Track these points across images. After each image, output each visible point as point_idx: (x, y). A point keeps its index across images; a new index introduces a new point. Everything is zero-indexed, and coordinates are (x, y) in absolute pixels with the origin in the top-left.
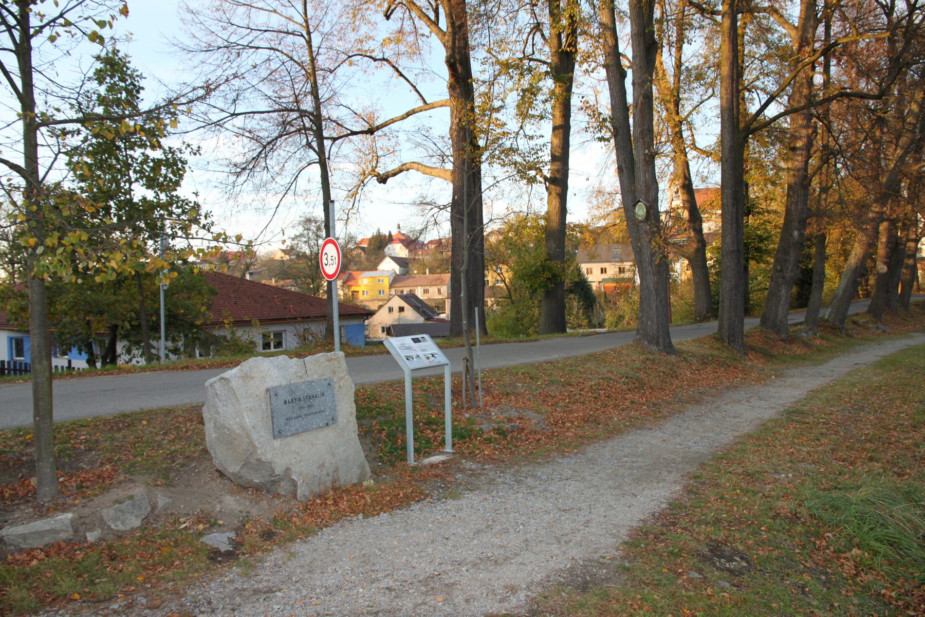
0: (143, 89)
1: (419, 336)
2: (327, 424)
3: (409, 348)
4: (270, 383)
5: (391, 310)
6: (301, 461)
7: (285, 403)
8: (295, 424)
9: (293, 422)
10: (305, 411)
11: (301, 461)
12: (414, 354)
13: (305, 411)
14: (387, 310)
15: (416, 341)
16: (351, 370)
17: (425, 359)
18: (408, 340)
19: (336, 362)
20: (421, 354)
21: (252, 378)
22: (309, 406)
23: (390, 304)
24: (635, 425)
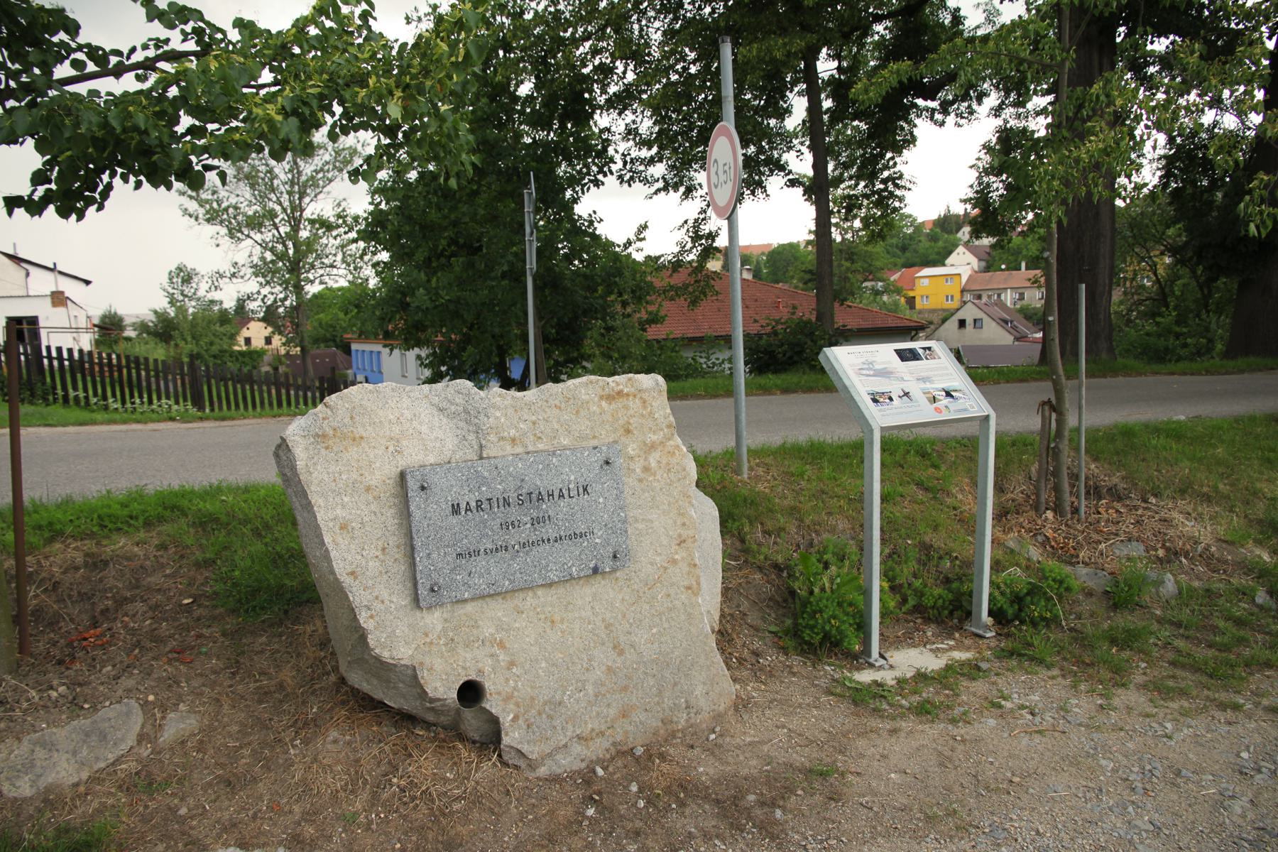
0: (961, 201)
1: (916, 345)
2: (596, 570)
3: (885, 373)
4: (413, 456)
5: (962, 323)
6: (512, 664)
7: (455, 510)
8: (489, 570)
9: (481, 562)
10: (525, 533)
11: (512, 664)
12: (895, 389)
13: (515, 537)
14: (957, 324)
15: (905, 356)
16: (682, 428)
17: (923, 401)
18: (885, 353)
19: (634, 404)
20: (915, 389)
21: (357, 440)
22: (536, 521)
23: (960, 315)
24: (571, 377)
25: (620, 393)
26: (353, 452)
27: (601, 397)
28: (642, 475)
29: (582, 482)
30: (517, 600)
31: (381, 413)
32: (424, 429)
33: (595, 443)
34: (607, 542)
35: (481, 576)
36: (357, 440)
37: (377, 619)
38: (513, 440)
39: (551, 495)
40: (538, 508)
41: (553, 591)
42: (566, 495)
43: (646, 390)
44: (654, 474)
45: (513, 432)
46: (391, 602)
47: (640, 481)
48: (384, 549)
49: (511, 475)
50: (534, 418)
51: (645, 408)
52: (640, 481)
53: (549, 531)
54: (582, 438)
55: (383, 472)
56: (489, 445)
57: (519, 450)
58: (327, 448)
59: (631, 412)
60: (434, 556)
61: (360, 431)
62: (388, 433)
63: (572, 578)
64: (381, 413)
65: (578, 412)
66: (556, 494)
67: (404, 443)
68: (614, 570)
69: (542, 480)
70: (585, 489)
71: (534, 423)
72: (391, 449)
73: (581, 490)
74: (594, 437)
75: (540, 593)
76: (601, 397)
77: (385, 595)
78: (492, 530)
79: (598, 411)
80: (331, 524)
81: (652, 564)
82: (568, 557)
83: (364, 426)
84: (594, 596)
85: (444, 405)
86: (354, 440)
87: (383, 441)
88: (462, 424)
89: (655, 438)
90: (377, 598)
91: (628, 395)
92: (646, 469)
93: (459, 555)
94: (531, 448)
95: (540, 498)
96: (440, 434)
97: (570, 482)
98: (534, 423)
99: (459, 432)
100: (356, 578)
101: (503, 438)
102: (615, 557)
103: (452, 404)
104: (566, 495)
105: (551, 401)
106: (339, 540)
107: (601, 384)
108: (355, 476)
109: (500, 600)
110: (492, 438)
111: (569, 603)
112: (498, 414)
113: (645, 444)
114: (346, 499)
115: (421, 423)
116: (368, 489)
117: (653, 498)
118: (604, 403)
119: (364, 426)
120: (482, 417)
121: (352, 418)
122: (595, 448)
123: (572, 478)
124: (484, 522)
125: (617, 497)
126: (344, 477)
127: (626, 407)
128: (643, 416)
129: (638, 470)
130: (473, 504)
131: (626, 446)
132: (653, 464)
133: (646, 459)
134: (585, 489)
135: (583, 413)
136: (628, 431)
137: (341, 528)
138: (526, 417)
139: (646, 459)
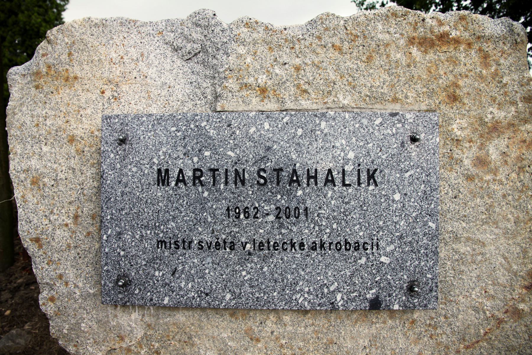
2: (375, 305)
4: (133, 103)
7: (163, 177)
8: (201, 270)
9: (192, 259)
10: (265, 228)
13: (247, 232)
21: (70, 80)
25: (443, 37)
26: (65, 94)
27: (411, 41)
28: (474, 171)
29: (365, 162)
30: (252, 323)
31: (102, 50)
32: (152, 72)
33: (396, 107)
34: (399, 265)
35: (190, 278)
36: (70, 80)
37: (58, 303)
38: (263, 91)
39: (312, 177)
40: (289, 193)
41: (309, 320)
42: (338, 181)
43: (489, 39)
44: (495, 172)
45: (262, 79)
46: (76, 286)
47: (470, 178)
48: (76, 217)
49: (251, 139)
50: (298, 61)
51: (486, 65)
52: (470, 178)
53: (306, 232)
54: (375, 98)
55: (88, 124)
56: (225, 93)
57: (271, 105)
58: (37, 87)
59: (462, 69)
60: (127, 237)
61: (76, 70)
62: (106, 75)
63: (334, 308)
64: (102, 50)
65: (370, 58)
66: (321, 177)
67: (124, 88)
68: (407, 309)
69: (299, 153)
70: (371, 176)
71: (298, 69)
72: (108, 94)
73: (364, 176)
74: (395, 100)
75: (287, 318)
76: (411, 41)
77: (71, 274)
78: (214, 216)
79: (404, 61)
80: (23, 176)
81: (476, 310)
82: (333, 275)
83: (81, 64)
84: (374, 339)
85: (179, 42)
86: (67, 79)
87: (100, 84)
88: (198, 68)
89: (500, 115)
90: (61, 277)
91: (457, 41)
92: (481, 162)
93: (161, 242)
94: (289, 105)
95: (294, 179)
96: (169, 78)
97: (347, 161)
98: (298, 69)
99: (194, 78)
100: (40, 247)
101: (246, 86)
102: (411, 289)
103: (189, 41)
104: (338, 181)
105: (326, 39)
106: (29, 196)
107: (411, 19)
108: (60, 122)
109: (228, 317)
110: (231, 83)
111: (332, 342)
112: (242, 50)
113: (481, 121)
114: (45, 149)
115: (149, 65)
116: (72, 140)
117: (489, 208)
118: (414, 50)
119: (81, 64)
120: (220, 55)
121: (70, 54)
122: (393, 115)
123: (351, 155)
124: (203, 202)
125: (426, 196)
126: (48, 122)
127: (454, 62)
128: (481, 76)
129: (466, 162)
130: (189, 173)
131: (449, 121)
132: (494, 155)
133: (482, 147)
134: (371, 176)
135: (377, 61)
136: (454, 98)
137: (33, 183)
138: (285, 59)
139: (482, 147)
